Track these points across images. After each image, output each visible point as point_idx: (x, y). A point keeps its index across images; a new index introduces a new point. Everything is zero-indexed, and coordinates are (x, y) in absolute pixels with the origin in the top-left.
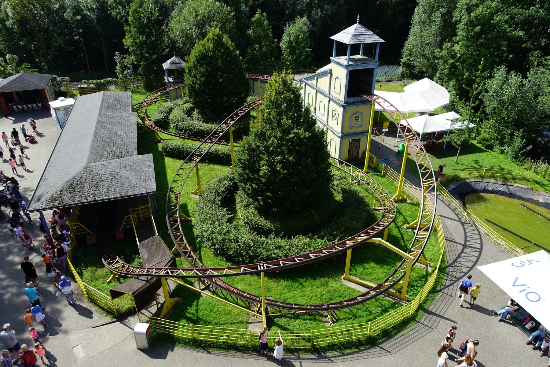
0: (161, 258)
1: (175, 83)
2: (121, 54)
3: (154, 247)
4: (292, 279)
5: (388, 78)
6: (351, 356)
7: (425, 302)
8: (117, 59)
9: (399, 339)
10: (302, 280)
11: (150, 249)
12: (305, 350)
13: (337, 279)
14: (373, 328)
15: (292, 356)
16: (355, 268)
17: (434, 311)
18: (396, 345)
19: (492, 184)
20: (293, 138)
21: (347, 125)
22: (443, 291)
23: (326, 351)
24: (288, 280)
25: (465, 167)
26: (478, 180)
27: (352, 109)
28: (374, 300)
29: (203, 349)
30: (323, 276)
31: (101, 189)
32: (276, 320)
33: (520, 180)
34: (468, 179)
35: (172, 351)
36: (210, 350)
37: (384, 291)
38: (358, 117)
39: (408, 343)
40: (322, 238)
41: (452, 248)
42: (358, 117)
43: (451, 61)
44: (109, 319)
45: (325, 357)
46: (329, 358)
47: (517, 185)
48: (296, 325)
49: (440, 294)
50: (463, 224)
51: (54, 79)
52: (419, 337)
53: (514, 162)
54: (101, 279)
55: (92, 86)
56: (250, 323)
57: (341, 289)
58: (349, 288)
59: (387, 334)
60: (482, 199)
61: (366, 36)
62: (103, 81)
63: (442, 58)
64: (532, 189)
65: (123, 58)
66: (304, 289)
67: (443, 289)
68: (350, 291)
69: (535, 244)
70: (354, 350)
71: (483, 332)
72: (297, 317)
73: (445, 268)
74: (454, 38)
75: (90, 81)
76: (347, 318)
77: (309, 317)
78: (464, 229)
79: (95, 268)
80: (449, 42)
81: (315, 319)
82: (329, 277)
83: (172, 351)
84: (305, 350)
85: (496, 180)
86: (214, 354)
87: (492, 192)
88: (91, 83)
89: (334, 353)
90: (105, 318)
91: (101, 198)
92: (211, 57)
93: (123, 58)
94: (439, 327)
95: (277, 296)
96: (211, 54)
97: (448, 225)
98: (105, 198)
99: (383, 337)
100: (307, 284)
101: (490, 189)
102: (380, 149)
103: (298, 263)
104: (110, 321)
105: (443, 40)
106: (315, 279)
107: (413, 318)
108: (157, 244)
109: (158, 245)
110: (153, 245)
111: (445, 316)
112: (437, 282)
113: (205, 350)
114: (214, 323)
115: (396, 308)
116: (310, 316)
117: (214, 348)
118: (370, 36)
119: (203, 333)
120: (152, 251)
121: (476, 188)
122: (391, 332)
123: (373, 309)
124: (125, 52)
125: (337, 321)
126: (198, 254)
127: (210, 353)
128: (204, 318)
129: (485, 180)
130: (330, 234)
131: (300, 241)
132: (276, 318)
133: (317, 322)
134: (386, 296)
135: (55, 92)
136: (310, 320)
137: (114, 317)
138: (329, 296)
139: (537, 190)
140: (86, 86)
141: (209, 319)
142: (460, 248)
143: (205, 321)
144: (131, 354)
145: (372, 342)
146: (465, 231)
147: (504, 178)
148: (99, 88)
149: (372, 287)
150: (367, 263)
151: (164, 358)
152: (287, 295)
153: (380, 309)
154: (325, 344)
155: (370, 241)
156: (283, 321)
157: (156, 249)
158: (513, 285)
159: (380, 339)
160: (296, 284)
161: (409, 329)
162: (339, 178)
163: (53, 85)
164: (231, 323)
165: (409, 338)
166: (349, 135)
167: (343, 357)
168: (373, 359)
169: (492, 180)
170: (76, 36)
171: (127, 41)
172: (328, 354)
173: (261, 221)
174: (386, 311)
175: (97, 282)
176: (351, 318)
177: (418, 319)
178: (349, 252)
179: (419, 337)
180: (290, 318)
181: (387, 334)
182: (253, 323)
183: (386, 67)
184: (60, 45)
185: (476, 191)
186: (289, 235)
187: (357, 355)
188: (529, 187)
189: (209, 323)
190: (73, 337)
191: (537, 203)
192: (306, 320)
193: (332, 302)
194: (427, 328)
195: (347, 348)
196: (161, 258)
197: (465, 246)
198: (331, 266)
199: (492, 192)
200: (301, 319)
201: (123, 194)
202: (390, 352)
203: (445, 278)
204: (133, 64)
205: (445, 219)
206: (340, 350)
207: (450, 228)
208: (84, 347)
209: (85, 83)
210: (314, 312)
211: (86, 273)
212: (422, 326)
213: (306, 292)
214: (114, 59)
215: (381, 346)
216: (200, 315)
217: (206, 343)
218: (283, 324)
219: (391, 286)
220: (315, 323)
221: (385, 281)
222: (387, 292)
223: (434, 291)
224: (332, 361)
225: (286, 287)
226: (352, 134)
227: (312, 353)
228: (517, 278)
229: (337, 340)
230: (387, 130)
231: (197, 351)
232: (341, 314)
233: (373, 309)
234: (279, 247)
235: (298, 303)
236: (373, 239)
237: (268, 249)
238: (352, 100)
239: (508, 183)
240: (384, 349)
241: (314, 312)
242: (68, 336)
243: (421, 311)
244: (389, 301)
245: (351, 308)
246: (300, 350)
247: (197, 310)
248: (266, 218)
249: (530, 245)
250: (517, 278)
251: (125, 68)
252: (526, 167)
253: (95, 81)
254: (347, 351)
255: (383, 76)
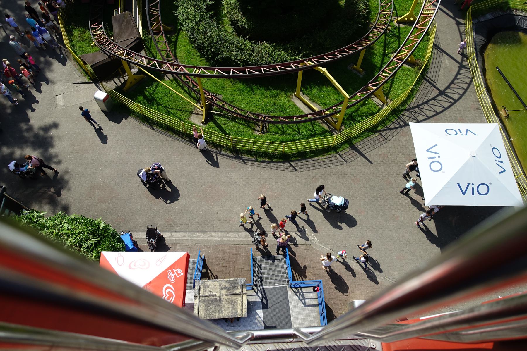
0: (129, 35)
3: (125, 23)
4: (247, 83)
6: (262, 163)
7: (356, 138)
9: (311, 162)
10: (255, 87)
11: (122, 24)
12: (227, 148)
13: (289, 94)
14: (291, 148)
15: (215, 150)
16: (311, 88)
17: (359, 148)
18: (305, 166)
22: (381, 133)
23: (244, 154)
24: (243, 84)
28: (309, 123)
29: (150, 124)
30: (276, 89)
32: (216, 117)
34: (517, 10)
35: (126, 119)
37: (324, 117)
39: (316, 168)
40: (286, 50)
44: (86, 79)
45: (241, 158)
46: (243, 160)
48: (231, 126)
49: (378, 134)
52: (329, 165)
54: (87, 42)
56: (194, 114)
57: (287, 104)
58: (295, 105)
59: (302, 155)
66: (253, 96)
67: (384, 130)
68: (294, 109)
70: (267, 160)
71: (390, 178)
72: (234, 119)
73: (402, 111)
76: (275, 133)
77: (244, 122)
79: (83, 29)
81: (248, 126)
82: (282, 90)
83: (126, 119)
84: (227, 148)
86: (156, 131)
89: (251, 158)
90: (84, 77)
94: (353, 163)
95: (227, 96)
99: (298, 156)
100: (259, 92)
104: (87, 81)
106: (267, 89)
107: (335, 149)
111: (366, 155)
112: (382, 122)
113: (151, 125)
114: (164, 105)
115: (324, 136)
116: (246, 121)
119: (151, 112)
120: (123, 27)
122: (307, 154)
123: (303, 131)
125: (267, 132)
126: (176, 36)
127: (153, 129)
128: (158, 100)
130: (297, 48)
131: (265, 47)
133: (249, 128)
134: (324, 122)
136: (244, 125)
137: (90, 79)
138: (272, 108)
141: (161, 102)
142: (436, 92)
143: (158, 102)
144: (96, 113)
145: (285, 158)
149: (315, 111)
150: (325, 85)
151: (119, 123)
152: (236, 97)
153: (310, 132)
154: (245, 148)
155: (316, 68)
156: (221, 120)
159: (294, 157)
160: (249, 89)
161: (325, 157)
164: (178, 110)
165: (319, 164)
167: (256, 163)
168: (279, 171)
172: (244, 157)
173: (238, 16)
174: (313, 136)
175: (83, 43)
176: (279, 133)
177: (338, 151)
178: (300, 73)
179: (329, 165)
181: (302, 155)
182: (196, 114)
186: (256, 38)
187: (267, 164)
189: (161, 105)
190: (58, 87)
192: (239, 123)
193: (272, 114)
194: (342, 160)
195: (262, 156)
197: (442, 93)
198: (284, 82)
200: (237, 122)
202: (296, 170)
203: (394, 120)
206: (256, 156)
208: (64, 98)
210: (249, 121)
211: (76, 33)
212: (339, 157)
213: (253, 99)
215: (292, 163)
216: (155, 96)
218: (220, 122)
219: (331, 115)
220: (247, 128)
221: (327, 110)
222: (325, 118)
223: (373, 130)
224: (245, 163)
225: (239, 89)
227: (232, 152)
228: (436, 145)
229: (256, 148)
231: (144, 125)
233: (303, 131)
234: (241, 50)
235: (242, 107)
236: (320, 68)
237: (230, 50)
240: (293, 166)
241: (249, 121)
242: (54, 85)
244: (323, 128)
245: (285, 125)
246: (223, 147)
247: (154, 91)
248: (244, 14)
250: (436, 145)
254: (261, 159)
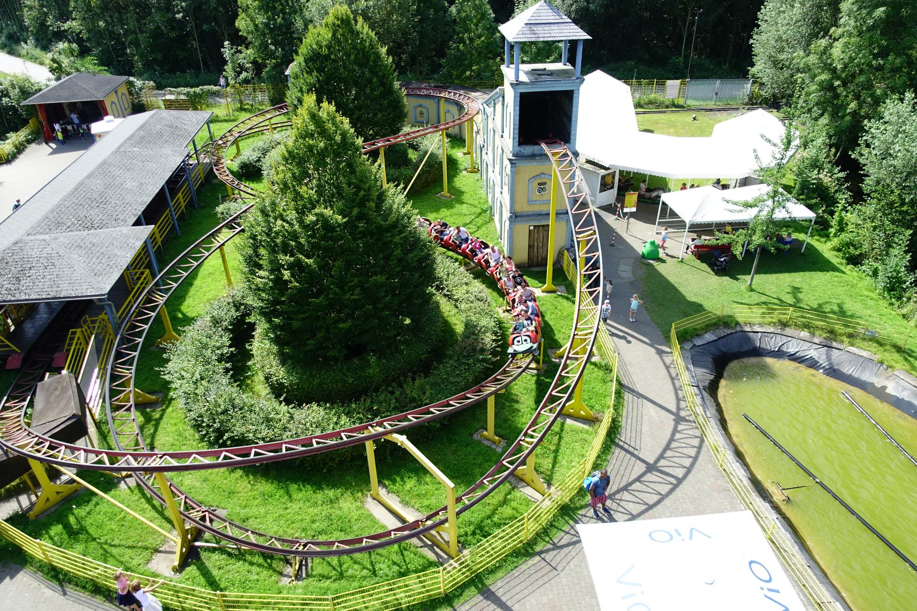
1: (871, 62)
2: (232, 44)
3: (57, 393)
5: (721, 105)
8: (227, 51)
10: (293, 487)
19: (798, 342)
20: (315, 223)
21: (521, 198)
25: (764, 299)
26: (772, 330)
27: (530, 169)
30: (334, 486)
31: (23, 282)
33: (864, 339)
36: (69, 589)
38: (545, 184)
41: (622, 468)
42: (545, 184)
43: (824, 77)
47: (852, 349)
49: (537, 558)
50: (679, 419)
51: (131, 84)
53: (884, 298)
55: (183, 97)
60: (767, 373)
61: (553, 27)
62: (197, 90)
63: (807, 69)
64: (882, 363)
65: (236, 52)
66: (289, 505)
68: (369, 523)
69: (821, 484)
72: (240, 556)
74: (833, 29)
75: (179, 89)
77: (261, 560)
78: (675, 431)
80: (823, 37)
81: (270, 567)
83: (12, 578)
85: (813, 334)
87: (793, 358)
88: (179, 94)
91: (18, 297)
92: (327, 57)
93: (236, 52)
96: (325, 51)
97: (645, 418)
98: (23, 297)
101: (792, 350)
102: (613, 245)
103: (285, 455)
105: (815, 36)
108: (62, 388)
109: (64, 390)
110: (56, 389)
113: (62, 586)
117: (77, 585)
118: (563, 26)
120: (53, 398)
121: (763, 346)
124: (238, 40)
129: (788, 331)
130: (370, 410)
131: (314, 413)
132: (205, 551)
134: (426, 545)
135: (133, 104)
136: (260, 565)
139: (889, 367)
140: (172, 97)
146: (673, 434)
147: (832, 332)
148: (194, 103)
153: (396, 568)
157: (59, 395)
158: (618, 581)
162: (473, 298)
163: (130, 93)
166: (528, 216)
169: (804, 334)
170: (179, 12)
171: (242, 23)
177: (456, 603)
180: (230, 555)
183: (718, 82)
184: (158, 27)
185: (758, 352)
188: (878, 357)
191: (880, 394)
196: (59, 413)
197: (651, 468)
199: (793, 358)
201: (52, 295)
204: (254, 62)
205: (649, 404)
207: (645, 425)
209: (171, 93)
214: (221, 54)
217: (66, 575)
226: (533, 215)
230: (634, 210)
232: (318, 566)
238: (529, 149)
239: (835, 344)
243: (473, 588)
249: (809, 482)
251: (241, 69)
252: (904, 311)
253: (188, 89)
255: (711, 99)
